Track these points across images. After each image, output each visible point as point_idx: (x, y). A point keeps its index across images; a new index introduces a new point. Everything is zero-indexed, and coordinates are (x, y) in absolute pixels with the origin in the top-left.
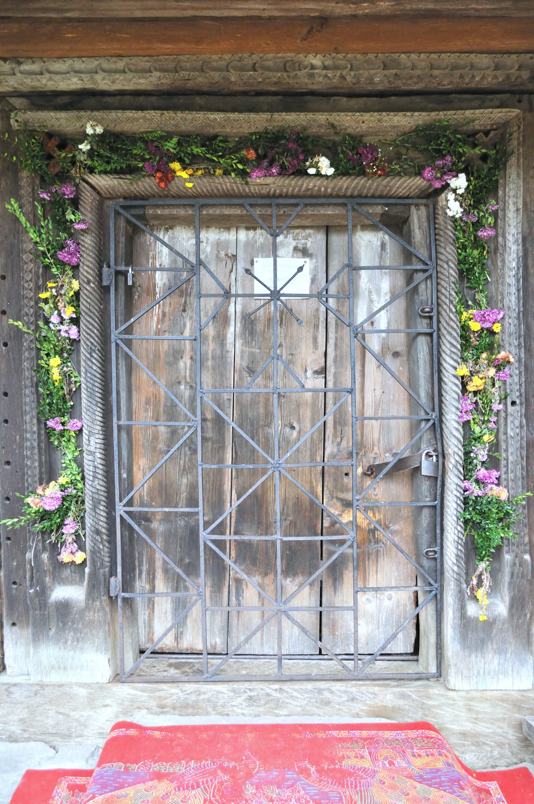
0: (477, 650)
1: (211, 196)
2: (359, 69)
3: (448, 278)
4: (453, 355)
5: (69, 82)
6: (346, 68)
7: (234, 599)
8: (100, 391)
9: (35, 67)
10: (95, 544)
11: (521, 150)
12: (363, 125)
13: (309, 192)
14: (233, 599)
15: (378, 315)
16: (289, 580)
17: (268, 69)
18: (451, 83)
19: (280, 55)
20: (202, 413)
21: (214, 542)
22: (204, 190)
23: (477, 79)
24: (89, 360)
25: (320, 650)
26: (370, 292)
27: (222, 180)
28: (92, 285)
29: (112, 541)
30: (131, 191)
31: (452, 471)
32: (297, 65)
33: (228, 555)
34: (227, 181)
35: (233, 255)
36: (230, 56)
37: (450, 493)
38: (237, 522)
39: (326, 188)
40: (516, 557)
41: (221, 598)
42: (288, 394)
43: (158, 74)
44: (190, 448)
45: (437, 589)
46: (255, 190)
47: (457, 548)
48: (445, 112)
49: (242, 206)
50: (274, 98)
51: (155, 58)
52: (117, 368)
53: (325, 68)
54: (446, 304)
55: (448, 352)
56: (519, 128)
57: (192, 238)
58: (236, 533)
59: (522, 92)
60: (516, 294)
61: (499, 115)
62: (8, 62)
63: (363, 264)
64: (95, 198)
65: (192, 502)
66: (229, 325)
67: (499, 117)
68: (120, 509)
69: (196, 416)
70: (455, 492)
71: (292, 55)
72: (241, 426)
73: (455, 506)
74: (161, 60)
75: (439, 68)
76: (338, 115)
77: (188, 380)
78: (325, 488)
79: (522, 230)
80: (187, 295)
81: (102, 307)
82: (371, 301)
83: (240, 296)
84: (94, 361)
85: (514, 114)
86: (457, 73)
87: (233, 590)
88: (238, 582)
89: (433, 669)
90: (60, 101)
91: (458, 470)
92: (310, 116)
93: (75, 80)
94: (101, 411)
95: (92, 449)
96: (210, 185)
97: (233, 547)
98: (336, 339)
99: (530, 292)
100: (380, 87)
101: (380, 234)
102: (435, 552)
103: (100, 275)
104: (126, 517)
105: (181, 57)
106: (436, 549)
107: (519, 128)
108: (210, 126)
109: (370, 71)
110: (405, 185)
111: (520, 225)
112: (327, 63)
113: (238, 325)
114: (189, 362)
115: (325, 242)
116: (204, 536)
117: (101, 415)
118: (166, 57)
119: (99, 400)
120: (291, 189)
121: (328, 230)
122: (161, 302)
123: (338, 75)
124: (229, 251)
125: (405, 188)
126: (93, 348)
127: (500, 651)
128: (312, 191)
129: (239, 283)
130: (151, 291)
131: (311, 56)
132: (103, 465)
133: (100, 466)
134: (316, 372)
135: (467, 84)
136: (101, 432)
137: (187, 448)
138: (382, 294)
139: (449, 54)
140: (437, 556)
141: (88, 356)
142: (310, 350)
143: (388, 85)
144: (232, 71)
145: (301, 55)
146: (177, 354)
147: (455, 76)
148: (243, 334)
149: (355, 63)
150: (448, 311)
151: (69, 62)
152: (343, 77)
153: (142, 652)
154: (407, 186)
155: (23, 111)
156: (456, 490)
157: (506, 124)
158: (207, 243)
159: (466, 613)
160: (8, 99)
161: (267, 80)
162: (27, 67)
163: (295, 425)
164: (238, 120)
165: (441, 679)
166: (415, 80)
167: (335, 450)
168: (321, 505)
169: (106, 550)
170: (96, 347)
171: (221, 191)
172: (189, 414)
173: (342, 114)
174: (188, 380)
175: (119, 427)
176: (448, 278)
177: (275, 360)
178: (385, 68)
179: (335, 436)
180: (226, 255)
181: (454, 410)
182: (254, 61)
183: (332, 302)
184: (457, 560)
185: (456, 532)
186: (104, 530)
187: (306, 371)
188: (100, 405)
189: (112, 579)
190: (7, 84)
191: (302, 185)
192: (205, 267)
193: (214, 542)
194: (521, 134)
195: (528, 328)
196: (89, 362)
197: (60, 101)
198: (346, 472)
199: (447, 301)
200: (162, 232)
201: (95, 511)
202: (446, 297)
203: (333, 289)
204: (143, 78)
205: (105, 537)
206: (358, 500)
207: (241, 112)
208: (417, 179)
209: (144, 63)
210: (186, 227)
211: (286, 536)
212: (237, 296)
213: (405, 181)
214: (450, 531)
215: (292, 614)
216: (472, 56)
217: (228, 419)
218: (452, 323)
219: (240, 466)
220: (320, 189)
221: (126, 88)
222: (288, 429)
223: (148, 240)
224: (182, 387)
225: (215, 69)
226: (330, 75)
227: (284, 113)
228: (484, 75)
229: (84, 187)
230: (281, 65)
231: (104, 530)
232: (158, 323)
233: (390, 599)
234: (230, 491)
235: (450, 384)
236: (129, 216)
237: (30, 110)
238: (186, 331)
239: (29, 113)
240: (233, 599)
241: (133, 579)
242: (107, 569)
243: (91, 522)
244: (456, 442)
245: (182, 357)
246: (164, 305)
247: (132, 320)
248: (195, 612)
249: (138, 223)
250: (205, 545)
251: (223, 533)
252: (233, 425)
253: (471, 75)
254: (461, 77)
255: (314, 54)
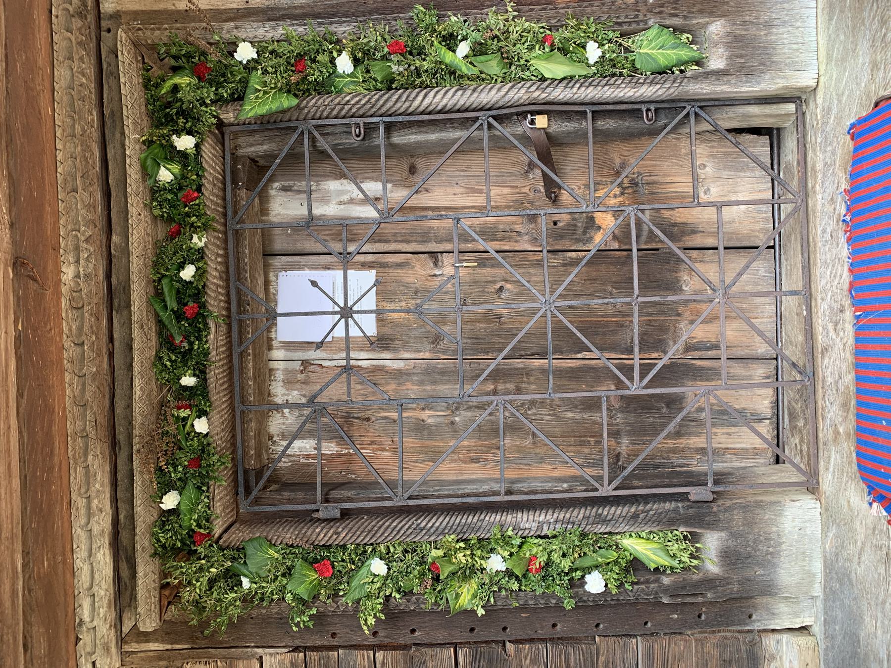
0: (771, 55)
1: (231, 390)
2: (77, 220)
3: (319, 107)
4: (411, 99)
5: (102, 563)
6: (76, 236)
7: (709, 352)
8: (465, 517)
9: (86, 604)
10: (649, 521)
11: (166, 26)
12: (142, 214)
13: (224, 276)
14: (710, 353)
15: (368, 193)
16: (684, 288)
17: (81, 328)
18: (90, 112)
19: (64, 315)
20: (488, 394)
21: (642, 377)
22: (224, 399)
23: (84, 81)
24: (429, 530)
25: (769, 247)
26: (340, 203)
27: (212, 379)
28: (340, 530)
29: (646, 499)
30: (228, 486)
31: (550, 94)
32: (75, 294)
33: (656, 361)
34: (213, 373)
35: (302, 364)
36: (66, 374)
37: (576, 96)
38: (616, 351)
39: (218, 255)
40: (651, 12)
41: (710, 368)
42: (462, 296)
43: (90, 458)
44: (529, 409)
45: (693, 107)
46: (223, 340)
47: (643, 83)
48: (125, 118)
49: (241, 355)
50: (115, 321)
51: (71, 462)
52: (438, 497)
53: (77, 261)
54: (351, 109)
55: (407, 104)
56: (140, 29)
57: (283, 413)
58: (630, 351)
59: (99, 27)
60: (336, 25)
61: (125, 53)
62: (81, 637)
63: (306, 212)
64: (238, 529)
65: (593, 404)
66: (384, 366)
67: (128, 54)
68: (607, 490)
69: (492, 402)
70: (575, 90)
71: (63, 300)
72: (501, 350)
73: (591, 88)
74: (74, 455)
75: (73, 126)
76: (132, 244)
77: (448, 413)
78: (573, 248)
79: (260, 21)
80: (349, 417)
81: (366, 517)
82: (351, 201)
83: (348, 354)
84: (430, 525)
85: (124, 35)
86: (78, 104)
87: (697, 354)
88: (688, 348)
89: (791, 107)
90: (125, 573)
91: (547, 87)
92: (134, 277)
93: (100, 556)
94: (489, 515)
95: (535, 525)
96: (219, 393)
97: (647, 356)
98: (396, 241)
99: (333, 10)
100: (99, 196)
101: (272, 192)
102: (648, 110)
103: (328, 521)
104: (616, 483)
105: (69, 431)
106: (644, 110)
107: (140, 29)
108: (149, 395)
109: (79, 208)
110: (211, 162)
111: (255, 25)
112: (72, 260)
113: (383, 356)
114: (428, 412)
115: (284, 258)
116: (636, 388)
117: (494, 515)
118: (70, 450)
119: (476, 518)
120: (220, 297)
121: (268, 254)
122: (358, 446)
123: (85, 245)
124: (297, 369)
125: (214, 162)
126: (414, 526)
127: (769, 25)
128: (223, 272)
129: (335, 357)
130: (346, 460)
131: (64, 278)
132: (553, 512)
133: (556, 515)
134: (436, 264)
135: (91, 93)
136: (515, 515)
137: (529, 412)
138: (341, 188)
139: (56, 115)
140: (652, 108)
141: (424, 532)
142: (410, 272)
143: (96, 186)
144: (84, 371)
145: (63, 290)
146: (420, 427)
147: (82, 106)
148: (396, 350)
149: (70, 227)
150: (358, 106)
151: (78, 563)
152: (87, 240)
153: (777, 461)
154: (213, 160)
155: (138, 616)
156: (572, 87)
157: (136, 44)
158: (288, 395)
159: (722, 70)
160: (123, 636)
161: (94, 328)
162: (86, 615)
163: (498, 286)
164: (142, 362)
165: (804, 97)
166: (87, 155)
167: (526, 238)
168: (592, 253)
169: (656, 506)
170: (413, 523)
171: (225, 379)
172: (489, 411)
173: (130, 239)
174: (448, 413)
175: (509, 492)
176: (319, 107)
177: (423, 310)
178: (75, 191)
179: (510, 239)
180: (302, 372)
181: (476, 95)
182: (72, 345)
183: (352, 248)
184: (657, 83)
185: (623, 85)
186: (633, 510)
187: (435, 275)
188: (482, 517)
189: (692, 498)
190: (106, 637)
191: (215, 284)
192: (315, 396)
193: (642, 377)
194: (147, 26)
195: (375, 11)
196: (432, 531)
197: (125, 573)
198: (552, 224)
199: (347, 108)
200: (277, 448)
201: (609, 521)
202: (342, 109)
203: (337, 247)
204: (95, 476)
205: (641, 508)
206: (588, 206)
207: (132, 359)
208: (203, 148)
209: (77, 477)
210: (270, 419)
211: (633, 288)
212: (348, 358)
213: (207, 162)
214: (621, 94)
215: (728, 280)
216: (57, 87)
217: (493, 365)
218: (373, 101)
219: (550, 348)
220: (219, 263)
221: (108, 495)
222: (504, 295)
223: (286, 465)
224: (457, 419)
225: (83, 390)
226: (86, 256)
227: (132, 308)
228: (78, 73)
229: (225, 541)
230: (76, 312)
231: (633, 510)
232: (383, 450)
233: (705, 166)
234: (578, 361)
235: (445, 101)
236: (257, 489)
237: (136, 608)
238: (392, 417)
239: (139, 610)
240: (710, 353)
241: (690, 474)
242: (680, 505)
243: (623, 525)
244: (515, 91)
245: (423, 421)
246: (362, 443)
247: (381, 481)
248: (727, 396)
249: (265, 477)
250: (646, 387)
251: (631, 368)
252: (499, 358)
253: (80, 88)
254: (82, 99)
255: (62, 274)
